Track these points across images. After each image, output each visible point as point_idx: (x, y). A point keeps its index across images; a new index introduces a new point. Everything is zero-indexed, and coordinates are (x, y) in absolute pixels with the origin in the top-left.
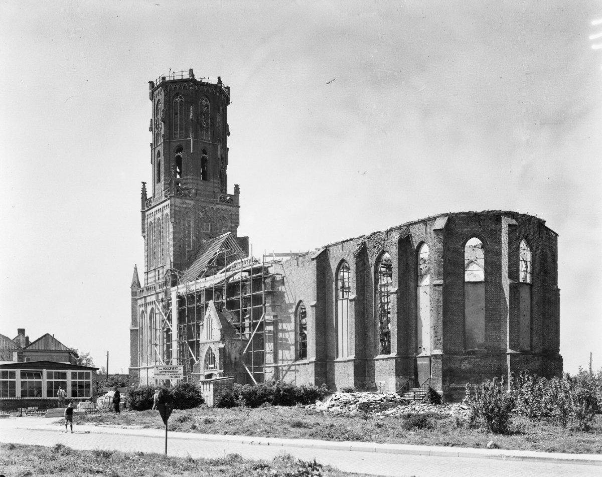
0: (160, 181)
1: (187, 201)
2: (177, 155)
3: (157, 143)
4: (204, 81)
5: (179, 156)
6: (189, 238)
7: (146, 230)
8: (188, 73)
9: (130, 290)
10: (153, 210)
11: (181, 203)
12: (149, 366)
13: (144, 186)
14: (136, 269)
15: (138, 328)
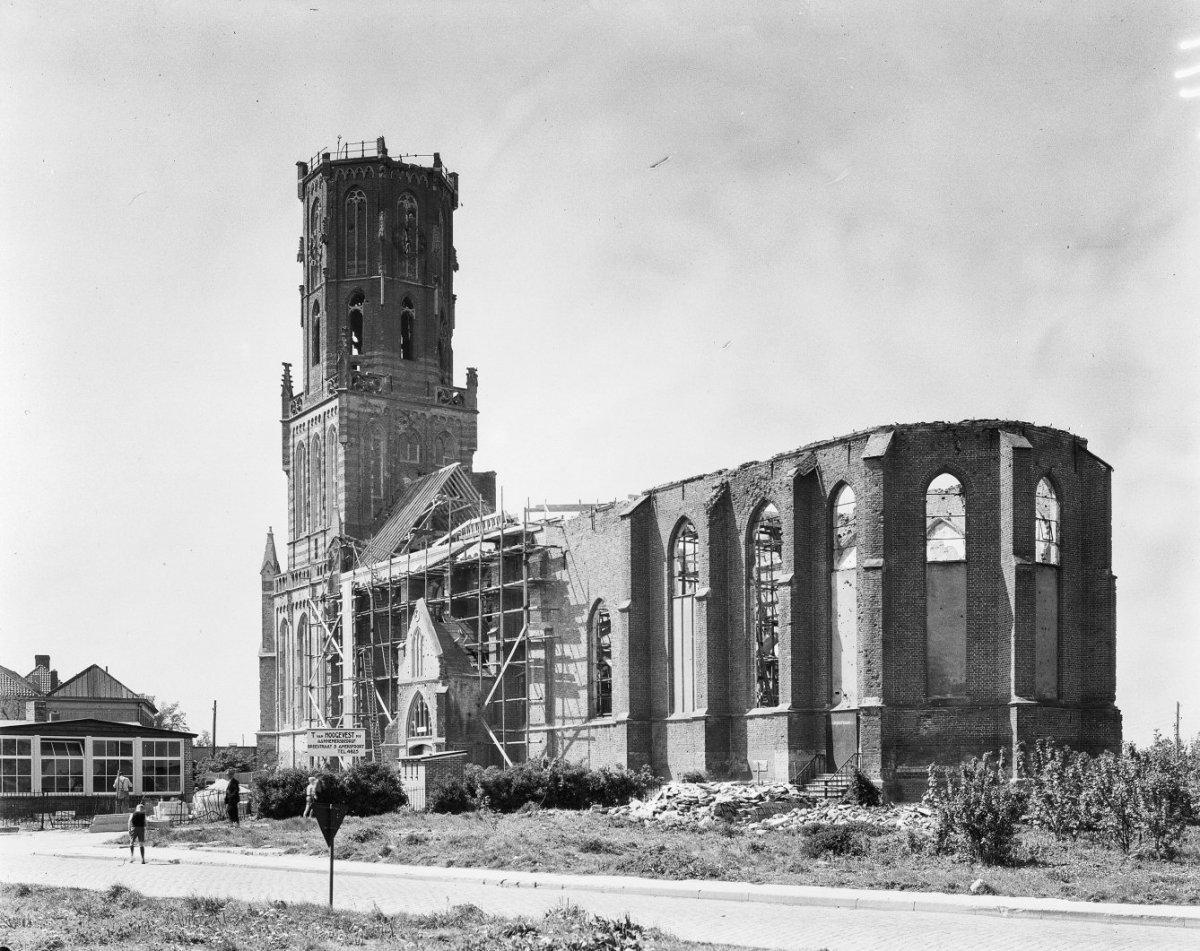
0: (318, 362)
1: (373, 401)
2: (352, 308)
3: (312, 285)
4: (406, 161)
5: (357, 311)
6: (377, 474)
7: (291, 458)
8: (375, 145)
9: (260, 577)
10: (305, 419)
11: (360, 406)
12: (297, 730)
13: (287, 371)
14: (271, 536)
15: (275, 654)
